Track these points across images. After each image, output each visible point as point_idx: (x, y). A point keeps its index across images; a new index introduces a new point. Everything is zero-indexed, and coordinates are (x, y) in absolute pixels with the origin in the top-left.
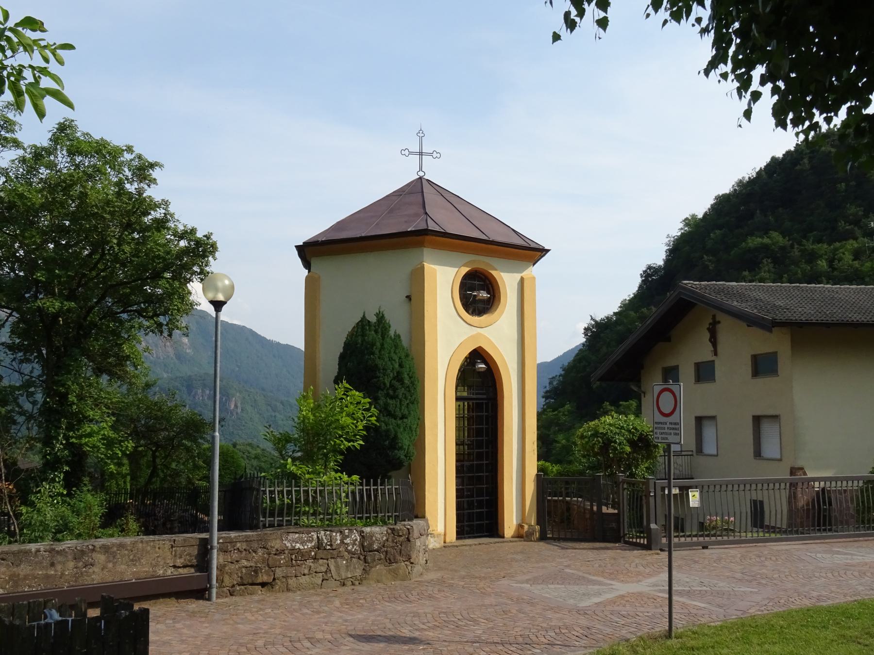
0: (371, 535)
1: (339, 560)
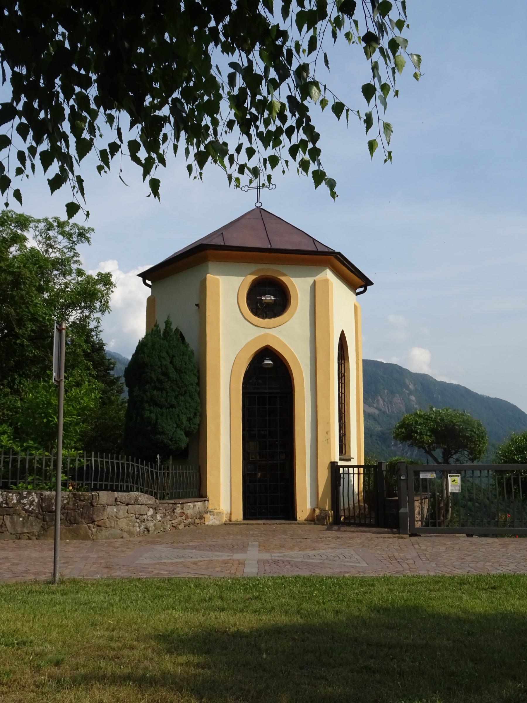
1: (15, 517)
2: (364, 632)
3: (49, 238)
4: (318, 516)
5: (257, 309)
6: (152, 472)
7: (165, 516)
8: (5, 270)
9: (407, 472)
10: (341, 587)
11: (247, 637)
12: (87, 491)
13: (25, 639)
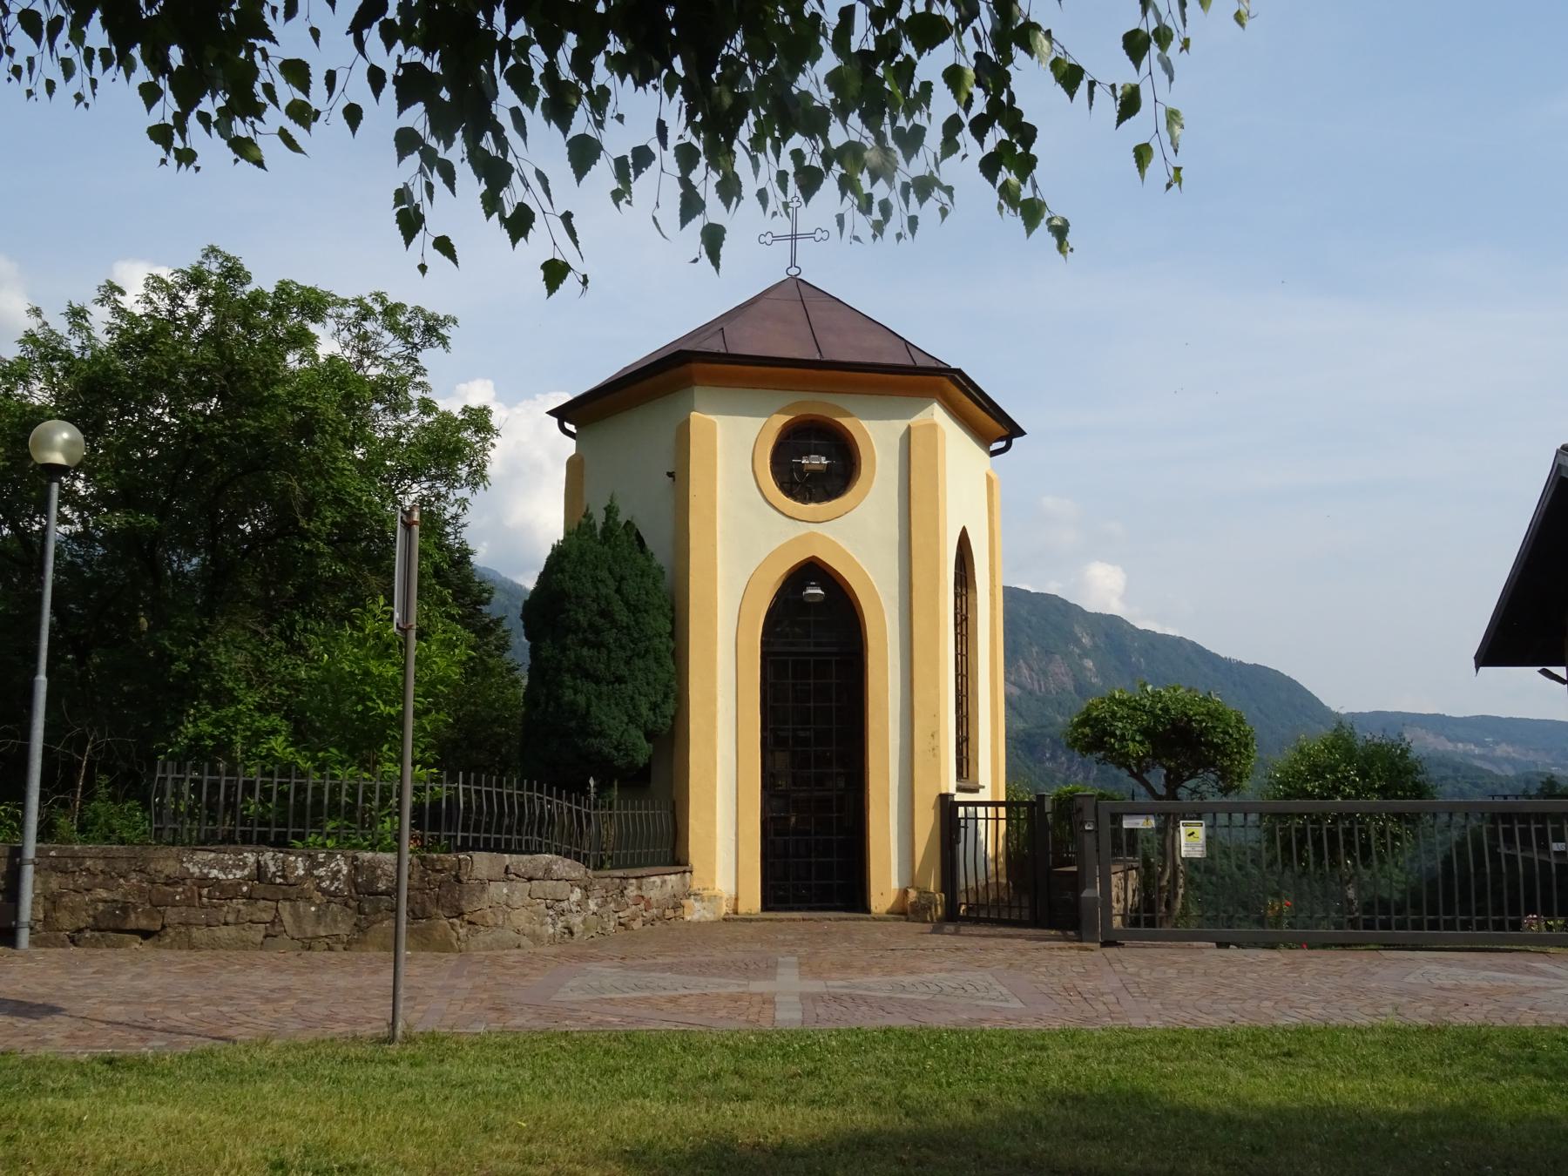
0: (373, 867)
1: (301, 904)
2: (1041, 1146)
3: (364, 337)
4: (913, 904)
5: (793, 482)
6: (578, 812)
7: (605, 903)
8: (284, 404)
9: (1097, 816)
10: (979, 1052)
11: (803, 1156)
12: (448, 852)
13: (352, 1160)
